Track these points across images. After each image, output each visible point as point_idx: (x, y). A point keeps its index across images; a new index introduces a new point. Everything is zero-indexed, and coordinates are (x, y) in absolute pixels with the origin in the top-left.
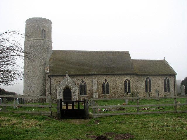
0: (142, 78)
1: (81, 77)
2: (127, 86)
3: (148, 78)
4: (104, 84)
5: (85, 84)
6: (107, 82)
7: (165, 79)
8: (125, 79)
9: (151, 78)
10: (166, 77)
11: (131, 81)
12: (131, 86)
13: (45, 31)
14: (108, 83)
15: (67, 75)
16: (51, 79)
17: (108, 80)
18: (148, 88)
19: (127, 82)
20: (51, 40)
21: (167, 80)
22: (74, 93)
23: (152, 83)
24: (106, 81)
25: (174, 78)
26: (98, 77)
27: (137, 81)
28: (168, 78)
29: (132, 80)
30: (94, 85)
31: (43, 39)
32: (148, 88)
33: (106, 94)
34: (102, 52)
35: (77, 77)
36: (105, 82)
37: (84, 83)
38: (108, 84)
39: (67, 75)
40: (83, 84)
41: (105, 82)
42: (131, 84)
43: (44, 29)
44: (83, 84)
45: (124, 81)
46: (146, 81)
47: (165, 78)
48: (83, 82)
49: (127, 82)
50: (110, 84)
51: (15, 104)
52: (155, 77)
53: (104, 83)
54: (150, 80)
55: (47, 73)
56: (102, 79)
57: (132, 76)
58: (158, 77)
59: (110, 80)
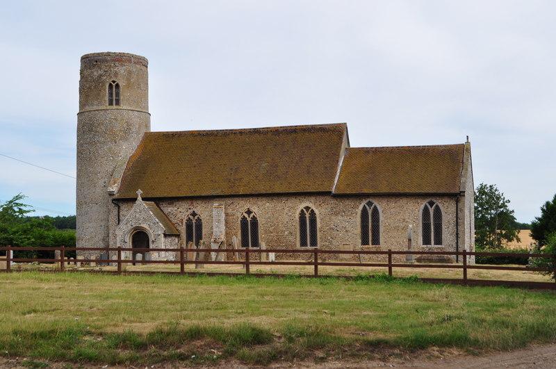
0: (349, 203)
1: (190, 202)
2: (308, 225)
3: (370, 204)
4: (244, 220)
5: (199, 220)
6: (251, 216)
7: (426, 207)
8: (302, 206)
9: (380, 205)
10: (368, 201)
11: (316, 211)
12: (319, 225)
13: (117, 86)
14: (254, 219)
15: (139, 198)
16: (122, 208)
17: (255, 209)
18: (370, 230)
19: (307, 215)
20: (147, 108)
21: (431, 211)
22: (153, 242)
23: (381, 218)
24: (249, 212)
25: (457, 202)
26: (229, 201)
27: (336, 214)
28: (438, 202)
29: (320, 209)
30: (215, 224)
31: (114, 107)
32: (370, 230)
33: (250, 248)
34: (267, 132)
35: (179, 204)
36: (246, 215)
37: (196, 218)
38: (255, 222)
39: (139, 198)
40: (194, 221)
41: (246, 215)
42: (318, 220)
43: (114, 82)
44: (194, 221)
45: (298, 212)
46: (364, 212)
47: (423, 203)
48: (194, 214)
49: (307, 215)
50: (261, 221)
51: (279, 344)
52: (393, 200)
53: (244, 219)
54: (375, 211)
55: (111, 194)
56: (240, 209)
57: (321, 199)
58: (403, 201)
59: (261, 210)
